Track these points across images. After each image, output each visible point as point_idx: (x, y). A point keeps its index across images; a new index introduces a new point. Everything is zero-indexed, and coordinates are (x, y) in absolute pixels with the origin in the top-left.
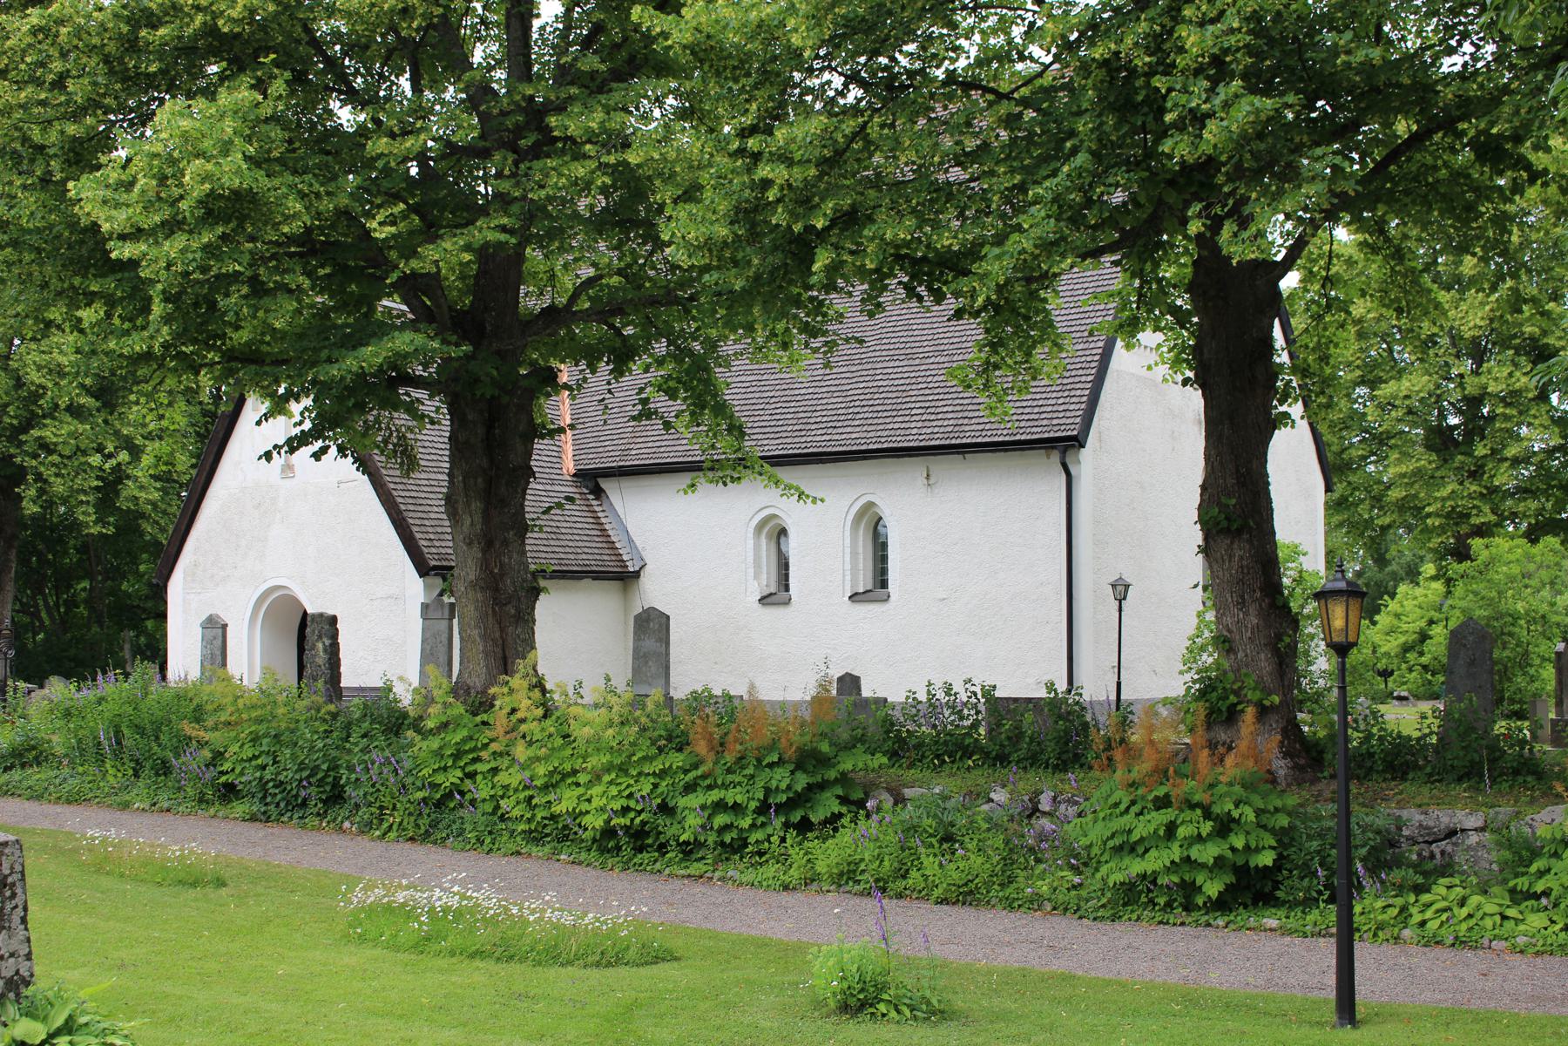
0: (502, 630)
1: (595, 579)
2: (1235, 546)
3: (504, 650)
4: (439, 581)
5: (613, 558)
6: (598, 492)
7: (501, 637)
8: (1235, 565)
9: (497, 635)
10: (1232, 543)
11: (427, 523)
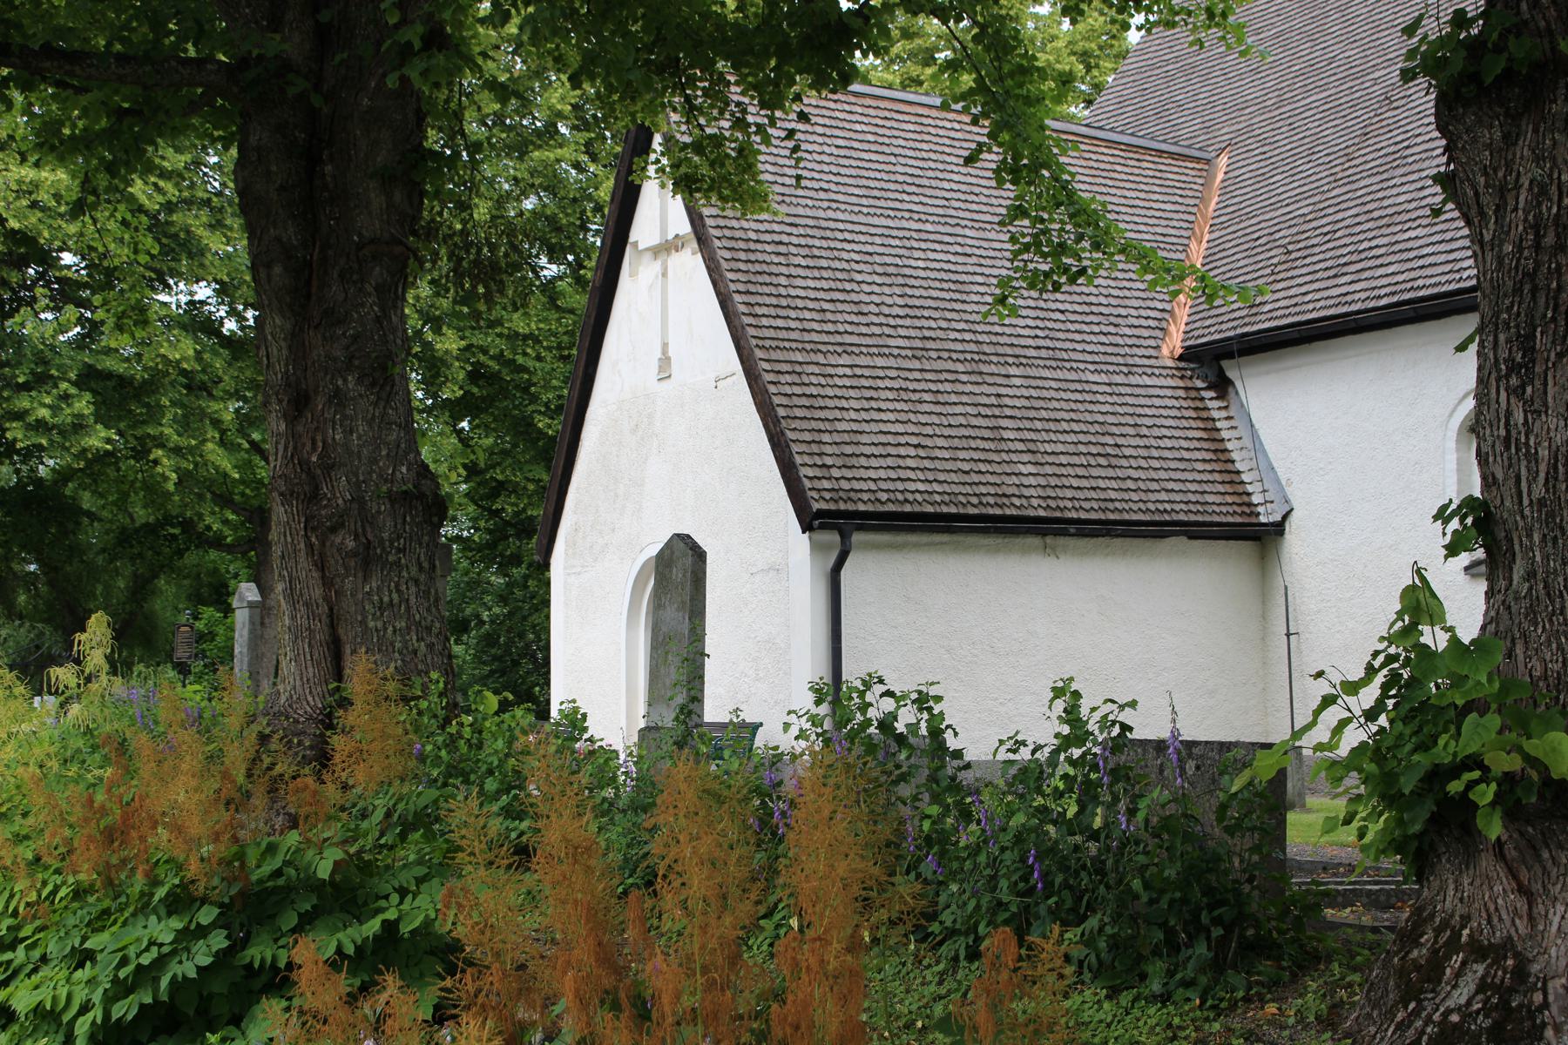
0: (327, 583)
1: (1192, 536)
2: (1523, 150)
3: (333, 627)
4: (834, 537)
5: (1237, 499)
6: (1222, 386)
7: (326, 599)
8: (1518, 221)
9: (317, 593)
10: (1510, 140)
11: (826, 438)
